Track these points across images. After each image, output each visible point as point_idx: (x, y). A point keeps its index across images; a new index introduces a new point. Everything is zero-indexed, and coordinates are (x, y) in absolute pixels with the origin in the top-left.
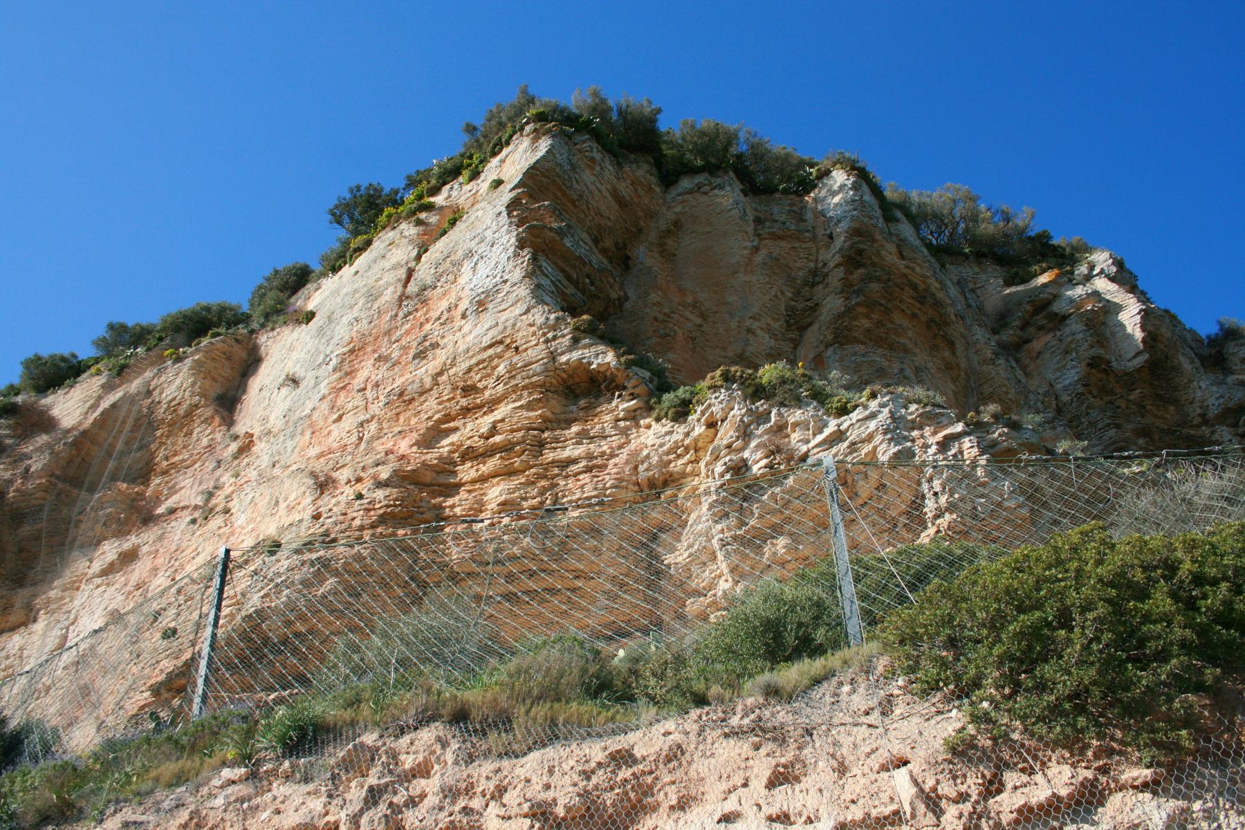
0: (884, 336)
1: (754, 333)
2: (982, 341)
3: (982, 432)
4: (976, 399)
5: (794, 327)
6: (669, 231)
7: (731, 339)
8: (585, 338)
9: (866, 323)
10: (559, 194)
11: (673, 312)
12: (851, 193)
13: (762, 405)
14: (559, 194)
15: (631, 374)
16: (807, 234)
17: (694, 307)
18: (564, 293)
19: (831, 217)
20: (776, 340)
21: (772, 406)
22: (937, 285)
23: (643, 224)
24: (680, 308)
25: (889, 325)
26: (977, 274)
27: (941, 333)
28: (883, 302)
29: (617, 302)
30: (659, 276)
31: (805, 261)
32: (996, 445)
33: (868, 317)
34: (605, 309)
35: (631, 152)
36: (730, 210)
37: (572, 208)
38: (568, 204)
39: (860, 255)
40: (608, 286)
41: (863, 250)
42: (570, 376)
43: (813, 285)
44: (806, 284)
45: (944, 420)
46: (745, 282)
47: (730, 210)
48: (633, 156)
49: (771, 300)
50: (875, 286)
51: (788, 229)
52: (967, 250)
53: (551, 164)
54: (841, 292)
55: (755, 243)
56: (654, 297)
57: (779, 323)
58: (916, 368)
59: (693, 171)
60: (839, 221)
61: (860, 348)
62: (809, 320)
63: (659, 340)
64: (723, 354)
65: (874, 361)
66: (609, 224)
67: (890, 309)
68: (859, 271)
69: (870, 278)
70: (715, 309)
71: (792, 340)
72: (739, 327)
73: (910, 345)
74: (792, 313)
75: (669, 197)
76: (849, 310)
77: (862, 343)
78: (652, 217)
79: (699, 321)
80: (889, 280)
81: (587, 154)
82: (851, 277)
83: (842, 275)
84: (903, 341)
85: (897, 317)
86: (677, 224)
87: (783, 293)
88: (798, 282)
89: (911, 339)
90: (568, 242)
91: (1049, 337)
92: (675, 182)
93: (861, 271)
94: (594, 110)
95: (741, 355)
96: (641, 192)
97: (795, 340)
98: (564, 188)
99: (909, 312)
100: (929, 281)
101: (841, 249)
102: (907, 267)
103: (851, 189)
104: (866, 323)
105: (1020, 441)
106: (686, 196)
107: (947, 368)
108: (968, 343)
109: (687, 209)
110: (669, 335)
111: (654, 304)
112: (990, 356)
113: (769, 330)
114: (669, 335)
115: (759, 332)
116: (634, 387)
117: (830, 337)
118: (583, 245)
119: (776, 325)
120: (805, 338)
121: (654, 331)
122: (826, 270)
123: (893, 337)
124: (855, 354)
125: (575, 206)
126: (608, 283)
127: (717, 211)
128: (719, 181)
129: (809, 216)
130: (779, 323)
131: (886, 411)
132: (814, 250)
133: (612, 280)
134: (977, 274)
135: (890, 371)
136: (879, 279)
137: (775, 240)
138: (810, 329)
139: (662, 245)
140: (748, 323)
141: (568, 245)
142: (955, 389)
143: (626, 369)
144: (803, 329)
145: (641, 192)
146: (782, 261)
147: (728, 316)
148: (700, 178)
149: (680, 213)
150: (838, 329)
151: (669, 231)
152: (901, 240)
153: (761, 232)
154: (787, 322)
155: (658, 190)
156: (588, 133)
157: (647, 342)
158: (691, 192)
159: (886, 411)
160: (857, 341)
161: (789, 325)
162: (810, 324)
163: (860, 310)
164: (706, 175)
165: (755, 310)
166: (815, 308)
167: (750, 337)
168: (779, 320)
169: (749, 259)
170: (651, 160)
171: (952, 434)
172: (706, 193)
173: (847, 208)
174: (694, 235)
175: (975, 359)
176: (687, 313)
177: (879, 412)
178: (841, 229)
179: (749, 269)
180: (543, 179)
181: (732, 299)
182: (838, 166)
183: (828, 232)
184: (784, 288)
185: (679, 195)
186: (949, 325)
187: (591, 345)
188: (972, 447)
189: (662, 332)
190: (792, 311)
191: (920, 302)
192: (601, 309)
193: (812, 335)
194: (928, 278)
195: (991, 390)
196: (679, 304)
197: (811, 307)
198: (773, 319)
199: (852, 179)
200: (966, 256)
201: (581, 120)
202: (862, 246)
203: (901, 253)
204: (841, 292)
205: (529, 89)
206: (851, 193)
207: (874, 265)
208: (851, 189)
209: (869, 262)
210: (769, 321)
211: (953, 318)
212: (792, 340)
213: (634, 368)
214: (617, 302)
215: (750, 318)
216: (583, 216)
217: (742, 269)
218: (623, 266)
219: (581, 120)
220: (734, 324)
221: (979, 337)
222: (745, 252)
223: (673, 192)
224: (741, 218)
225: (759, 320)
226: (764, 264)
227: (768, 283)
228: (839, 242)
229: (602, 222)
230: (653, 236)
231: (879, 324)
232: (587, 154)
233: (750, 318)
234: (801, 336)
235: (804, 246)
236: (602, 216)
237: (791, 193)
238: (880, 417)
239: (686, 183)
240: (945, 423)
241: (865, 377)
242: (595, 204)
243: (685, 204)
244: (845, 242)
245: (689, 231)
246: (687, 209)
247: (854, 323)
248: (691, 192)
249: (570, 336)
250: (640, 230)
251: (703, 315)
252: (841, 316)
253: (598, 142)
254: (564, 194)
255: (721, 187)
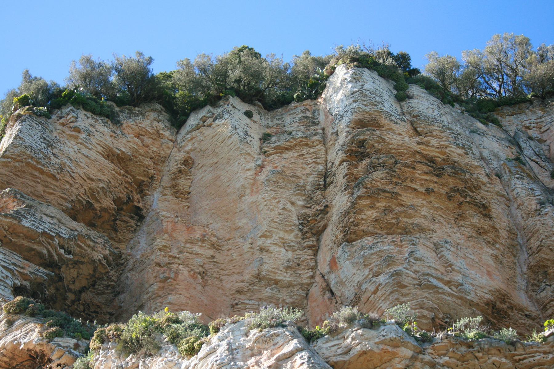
0: (394, 221)
1: (267, 251)
2: (523, 193)
3: (338, 339)
4: (526, 256)
5: (308, 235)
6: (180, 171)
7: (246, 262)
8: (18, 319)
9: (372, 214)
10: (36, 173)
11: (181, 252)
12: (350, 86)
13: (131, 359)
14: (36, 173)
15: (53, 347)
16: (316, 138)
17: (203, 241)
18: (22, 274)
19: (336, 115)
20: (294, 251)
21: (138, 359)
22: (461, 151)
23: (152, 172)
24: (188, 245)
25: (398, 209)
26: (541, 118)
27: (468, 199)
28: (388, 188)
29: (104, 262)
30: (165, 220)
31: (313, 165)
32: (350, 350)
33: (372, 207)
34: (95, 271)
35: (135, 106)
36: (230, 137)
37: (54, 182)
38: (49, 180)
39: (363, 146)
40: (89, 250)
41: (364, 141)
42: (12, 359)
43: (325, 186)
44: (317, 187)
45: (280, 340)
46: (252, 203)
47: (230, 137)
48: (137, 109)
49: (280, 214)
50: (378, 174)
51: (294, 139)
52: (530, 96)
53: (19, 149)
54: (346, 189)
55: (259, 162)
56: (159, 242)
57: (293, 234)
58: (435, 244)
59: (197, 106)
60: (342, 117)
61: (368, 241)
62: (323, 223)
63: (161, 285)
64: (241, 278)
65: (382, 251)
66: (101, 185)
67: (396, 194)
68: (364, 162)
69: (373, 167)
70: (228, 236)
71: (310, 247)
72: (251, 248)
73: (425, 223)
74: (304, 220)
75: (180, 137)
76: (354, 204)
77: (372, 234)
78: (164, 162)
79: (211, 252)
80: (396, 163)
81: (72, 125)
82: (355, 171)
83: (345, 171)
84: (417, 221)
85: (407, 198)
86: (188, 162)
87: (293, 203)
88: (308, 188)
89: (425, 217)
90: (26, 223)
91: (283, 250)
92: (185, 121)
93: (367, 161)
94: (86, 77)
95: (258, 275)
96: (148, 141)
97: (313, 246)
98: (39, 166)
99: (422, 190)
100: (448, 150)
101: (343, 146)
102: (419, 143)
103: (351, 81)
104: (372, 214)
105: (377, 340)
106: (193, 133)
107: (480, 234)
108: (509, 200)
109: (196, 145)
110: (169, 278)
111: (160, 250)
112: (534, 207)
113: (285, 245)
114: (169, 278)
115: (272, 248)
116: (59, 358)
117: (341, 237)
118: (49, 220)
119: (290, 237)
120: (323, 241)
121: (156, 277)
122: (333, 170)
123: (405, 220)
124: (363, 248)
125: (57, 180)
126: (89, 246)
127: (221, 140)
128: (219, 110)
129: (321, 118)
130: (293, 234)
131: (224, 343)
132: (323, 151)
133: (92, 244)
134: (541, 118)
135: (400, 257)
136: (383, 166)
137: (281, 153)
138: (325, 232)
139: (175, 186)
140: (260, 242)
141: (28, 225)
142: (495, 252)
143: (48, 342)
144: (319, 233)
145: (148, 141)
146: (288, 172)
147: (241, 240)
148: (203, 112)
149: (191, 150)
150: (345, 227)
151: (180, 171)
152: (414, 117)
153: (266, 149)
154: (301, 230)
155: (167, 134)
156: (72, 104)
157: (150, 289)
158: (197, 127)
159: (224, 343)
160: (367, 233)
161: (304, 234)
162: (325, 227)
163: (363, 202)
164: (208, 108)
165: (264, 228)
166: (325, 210)
167: (265, 256)
168: (292, 231)
169: (255, 179)
170: (158, 107)
171: (284, 354)
172: (210, 126)
173: (347, 103)
174: (204, 168)
175: (518, 214)
176: (197, 249)
177: (219, 346)
178: (343, 126)
179: (254, 189)
180: (17, 164)
181: (243, 222)
182: (340, 62)
183: (335, 130)
184: (293, 199)
185: (187, 133)
186: (479, 188)
187: (24, 325)
188: (302, 364)
189: (161, 276)
190: (305, 219)
191: (437, 175)
192: (91, 272)
193: (328, 237)
194: (446, 147)
195: (538, 243)
196: (186, 242)
197: (321, 211)
198: (286, 231)
199: (351, 71)
200: (531, 102)
201: (63, 94)
202: (362, 137)
203: (415, 129)
204: (346, 189)
205: (30, 72)
206: (350, 86)
207: (378, 152)
208: (351, 81)
209: (372, 151)
210: (282, 234)
211: (485, 179)
212: (310, 247)
213: (56, 339)
214: (104, 262)
215: (262, 236)
216: (68, 186)
217: (248, 191)
218: (137, 218)
219: (63, 94)
220: (246, 247)
221: (519, 190)
222: (249, 173)
223: (183, 131)
224: (241, 142)
225: (271, 237)
226: (268, 180)
227: (275, 198)
228: (343, 139)
229: (93, 185)
230: (166, 180)
231: (388, 210)
232: (72, 125)
233: (262, 236)
234: (318, 240)
235: (312, 150)
236: (92, 180)
237: (305, 99)
238: (219, 352)
239: (193, 120)
240: (280, 343)
241: (375, 269)
242: (80, 171)
243: (194, 141)
244: (346, 137)
245: (200, 166)
246: (196, 145)
247: (359, 217)
248: (197, 127)
249: (4, 321)
250: (152, 178)
251: (213, 246)
252: (347, 213)
253: (86, 110)
254: (42, 172)
255: (220, 117)
